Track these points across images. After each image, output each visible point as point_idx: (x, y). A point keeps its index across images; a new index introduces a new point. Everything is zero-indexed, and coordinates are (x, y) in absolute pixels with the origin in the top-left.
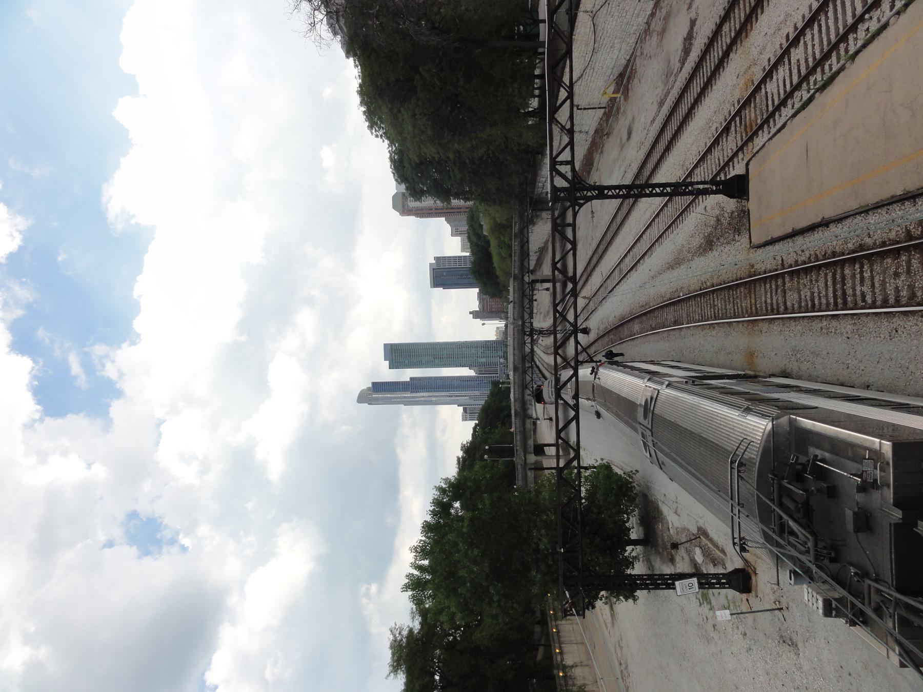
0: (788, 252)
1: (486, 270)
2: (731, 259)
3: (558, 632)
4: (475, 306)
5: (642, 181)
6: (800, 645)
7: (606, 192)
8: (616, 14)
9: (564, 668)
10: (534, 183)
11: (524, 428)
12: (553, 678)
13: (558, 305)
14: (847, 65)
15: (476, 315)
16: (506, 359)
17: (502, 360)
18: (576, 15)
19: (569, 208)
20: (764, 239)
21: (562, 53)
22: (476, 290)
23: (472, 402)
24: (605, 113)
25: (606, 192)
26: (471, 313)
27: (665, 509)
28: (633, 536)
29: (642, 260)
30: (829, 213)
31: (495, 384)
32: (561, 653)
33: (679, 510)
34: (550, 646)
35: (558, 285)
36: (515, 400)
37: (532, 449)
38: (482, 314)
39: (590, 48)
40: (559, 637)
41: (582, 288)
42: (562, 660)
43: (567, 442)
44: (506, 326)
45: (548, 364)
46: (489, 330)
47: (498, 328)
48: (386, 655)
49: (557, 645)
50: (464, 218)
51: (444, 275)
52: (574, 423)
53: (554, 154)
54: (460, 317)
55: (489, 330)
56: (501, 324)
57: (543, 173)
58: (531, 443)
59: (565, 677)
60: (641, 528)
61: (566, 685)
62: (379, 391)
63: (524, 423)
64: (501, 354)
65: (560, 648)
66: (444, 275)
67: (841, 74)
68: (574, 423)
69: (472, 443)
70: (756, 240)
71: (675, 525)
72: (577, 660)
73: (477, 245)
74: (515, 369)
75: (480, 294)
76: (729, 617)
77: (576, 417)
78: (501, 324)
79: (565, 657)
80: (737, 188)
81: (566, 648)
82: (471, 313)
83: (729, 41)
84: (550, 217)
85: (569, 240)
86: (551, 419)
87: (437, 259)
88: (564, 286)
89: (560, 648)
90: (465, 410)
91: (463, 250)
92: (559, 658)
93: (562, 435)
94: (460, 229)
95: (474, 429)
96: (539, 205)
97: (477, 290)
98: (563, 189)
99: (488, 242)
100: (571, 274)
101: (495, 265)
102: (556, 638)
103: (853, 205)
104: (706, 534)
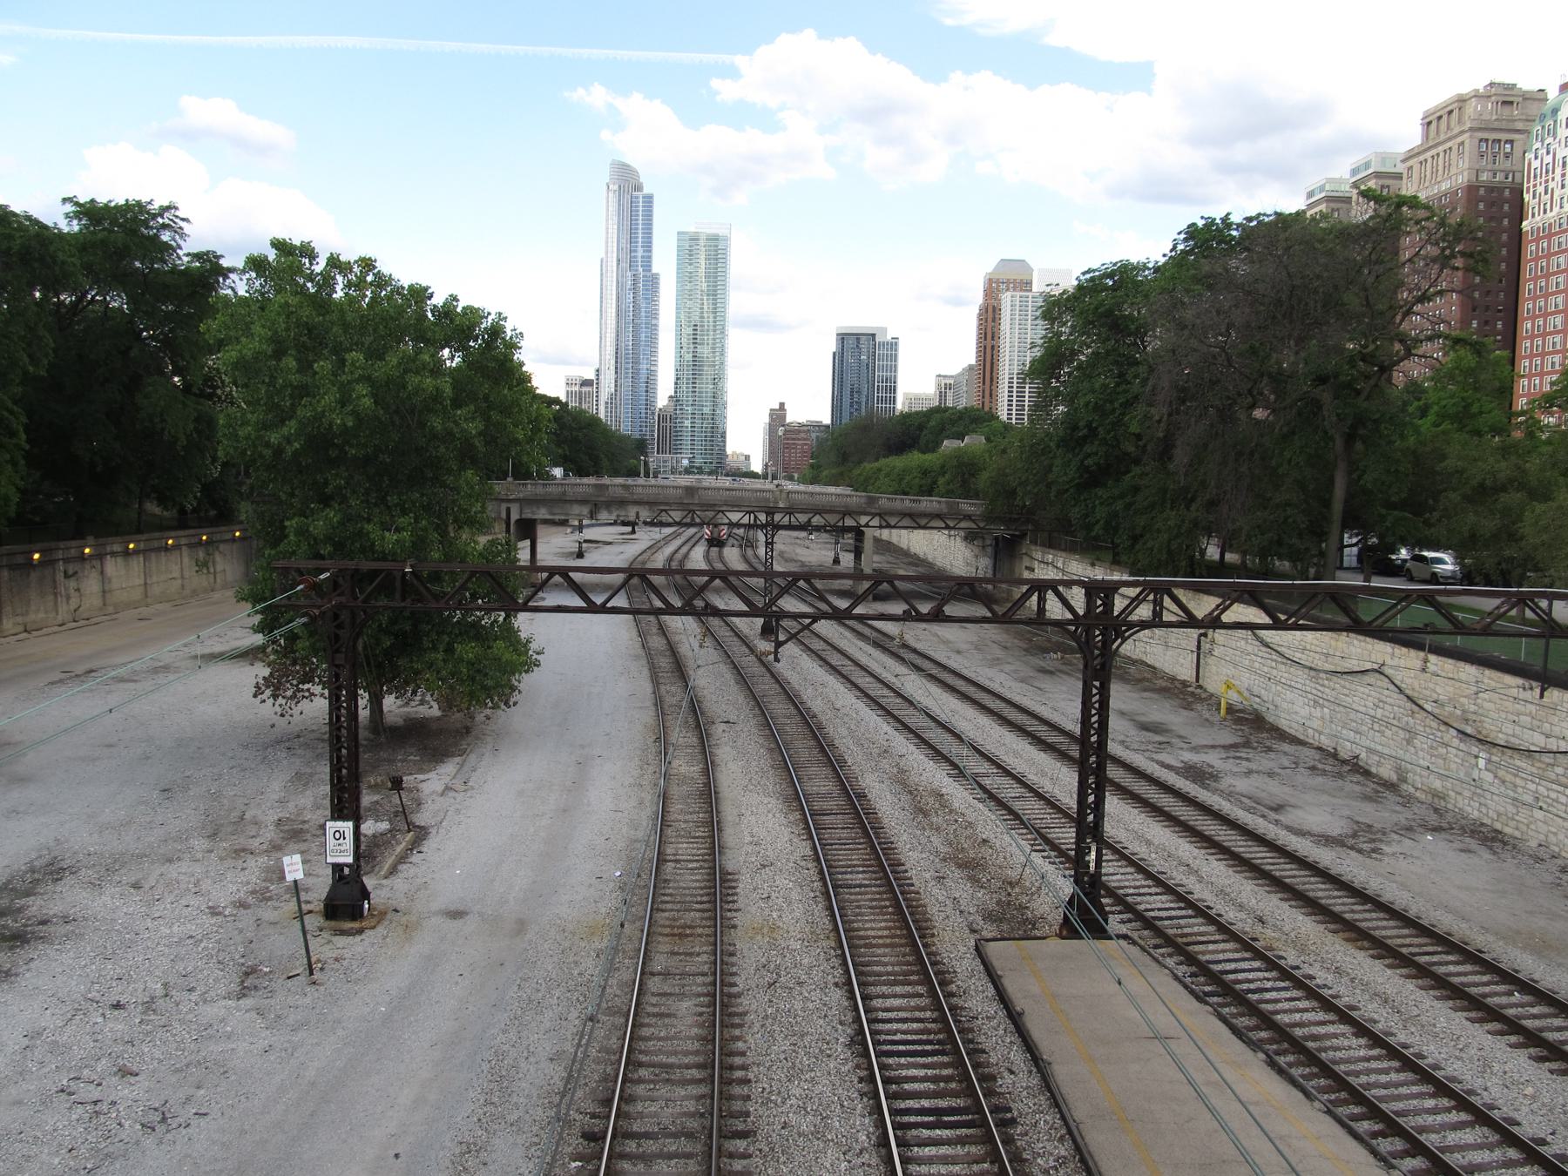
0: (978, 1001)
1: (871, 444)
2: (951, 907)
3: (167, 549)
4: (794, 416)
5: (1075, 751)
6: (247, 1002)
7: (1097, 684)
8: (1379, 711)
9: (99, 556)
10: (1051, 544)
11: (570, 502)
12: (79, 535)
13: (808, 581)
14: (1317, 1104)
15: (778, 415)
16: (688, 471)
17: (685, 462)
18: (1419, 647)
19: (991, 610)
20: (997, 964)
21: (1293, 610)
22: (826, 419)
23: (604, 397)
24: (1184, 683)
25: (1097, 684)
26: (782, 405)
27: (448, 768)
28: (389, 702)
29: (945, 739)
30: (1062, 1073)
31: (641, 446)
32: (127, 553)
33: (452, 794)
34: (139, 531)
35: (847, 584)
36: (626, 487)
37: (528, 515)
38: (782, 435)
39: (1320, 663)
40: (158, 550)
41: (853, 630)
42: (113, 554)
43: (541, 587)
44: (754, 475)
45: (686, 556)
46: (746, 441)
47: (747, 458)
48: (113, 191)
49: (142, 546)
50: (964, 400)
51: (861, 361)
52: (581, 603)
53: (1176, 591)
54: (773, 387)
55: (746, 441)
56: (757, 466)
57: (1074, 564)
58: (542, 513)
59: (82, 558)
60: (400, 722)
61: (66, 560)
62: (633, 206)
63: (583, 502)
64: (698, 462)
65: (136, 552)
66: (861, 361)
67: (1300, 1095)
68: (581, 603)
69: (532, 390)
70: (993, 949)
71: (423, 786)
72: (115, 584)
73: (921, 427)
74: (690, 491)
75: (818, 426)
76: (290, 878)
77: (592, 608)
78: (757, 466)
79: (119, 560)
80: (1087, 915)
81: (137, 564)
82: (782, 405)
83: (1337, 909)
84: (981, 574)
85: (853, 606)
86: (580, 555)
87: (893, 345)
88: (842, 594)
89: (136, 552)
90: (586, 383)
91: (910, 399)
92: (117, 548)
93: (557, 578)
94: (950, 394)
95: (557, 401)
96: (1005, 550)
97: (827, 420)
98: (1109, 605)
99: (933, 451)
100: (949, 610)
101: (883, 462)
102: (156, 544)
103: (1079, 1111)
104: (415, 844)
